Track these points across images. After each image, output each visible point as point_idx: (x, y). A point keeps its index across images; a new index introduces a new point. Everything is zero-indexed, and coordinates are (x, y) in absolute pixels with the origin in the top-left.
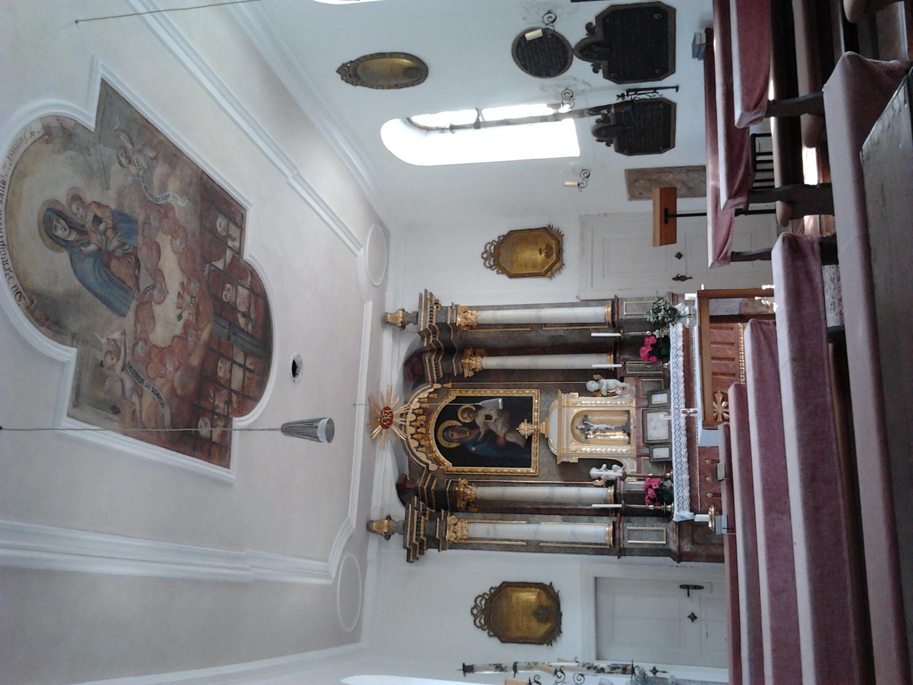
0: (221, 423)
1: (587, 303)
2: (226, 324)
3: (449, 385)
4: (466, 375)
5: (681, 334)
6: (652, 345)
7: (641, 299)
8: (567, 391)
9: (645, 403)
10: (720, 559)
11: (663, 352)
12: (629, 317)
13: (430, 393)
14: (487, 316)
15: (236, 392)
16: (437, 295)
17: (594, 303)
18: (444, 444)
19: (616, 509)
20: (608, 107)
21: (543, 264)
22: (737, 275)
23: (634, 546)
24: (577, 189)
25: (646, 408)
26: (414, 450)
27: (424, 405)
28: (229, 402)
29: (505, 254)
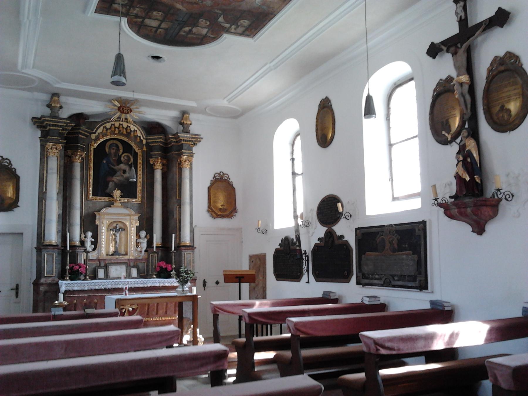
0: (124, 10)
1: (192, 231)
2: (185, 20)
3: (145, 149)
4: (151, 159)
5: (173, 285)
6: (166, 268)
7: (193, 262)
8: (140, 219)
9: (132, 264)
10: (35, 310)
11: (162, 275)
12: (183, 255)
13: (140, 137)
14: (186, 173)
15: (143, 20)
16: (199, 145)
17: (192, 235)
18: (108, 144)
19: (67, 247)
20: (300, 245)
21: (216, 207)
22: (205, 316)
23: (43, 257)
24: (257, 227)
25: (129, 265)
26: (104, 126)
27: (132, 133)
28: (137, 16)
29: (221, 185)
